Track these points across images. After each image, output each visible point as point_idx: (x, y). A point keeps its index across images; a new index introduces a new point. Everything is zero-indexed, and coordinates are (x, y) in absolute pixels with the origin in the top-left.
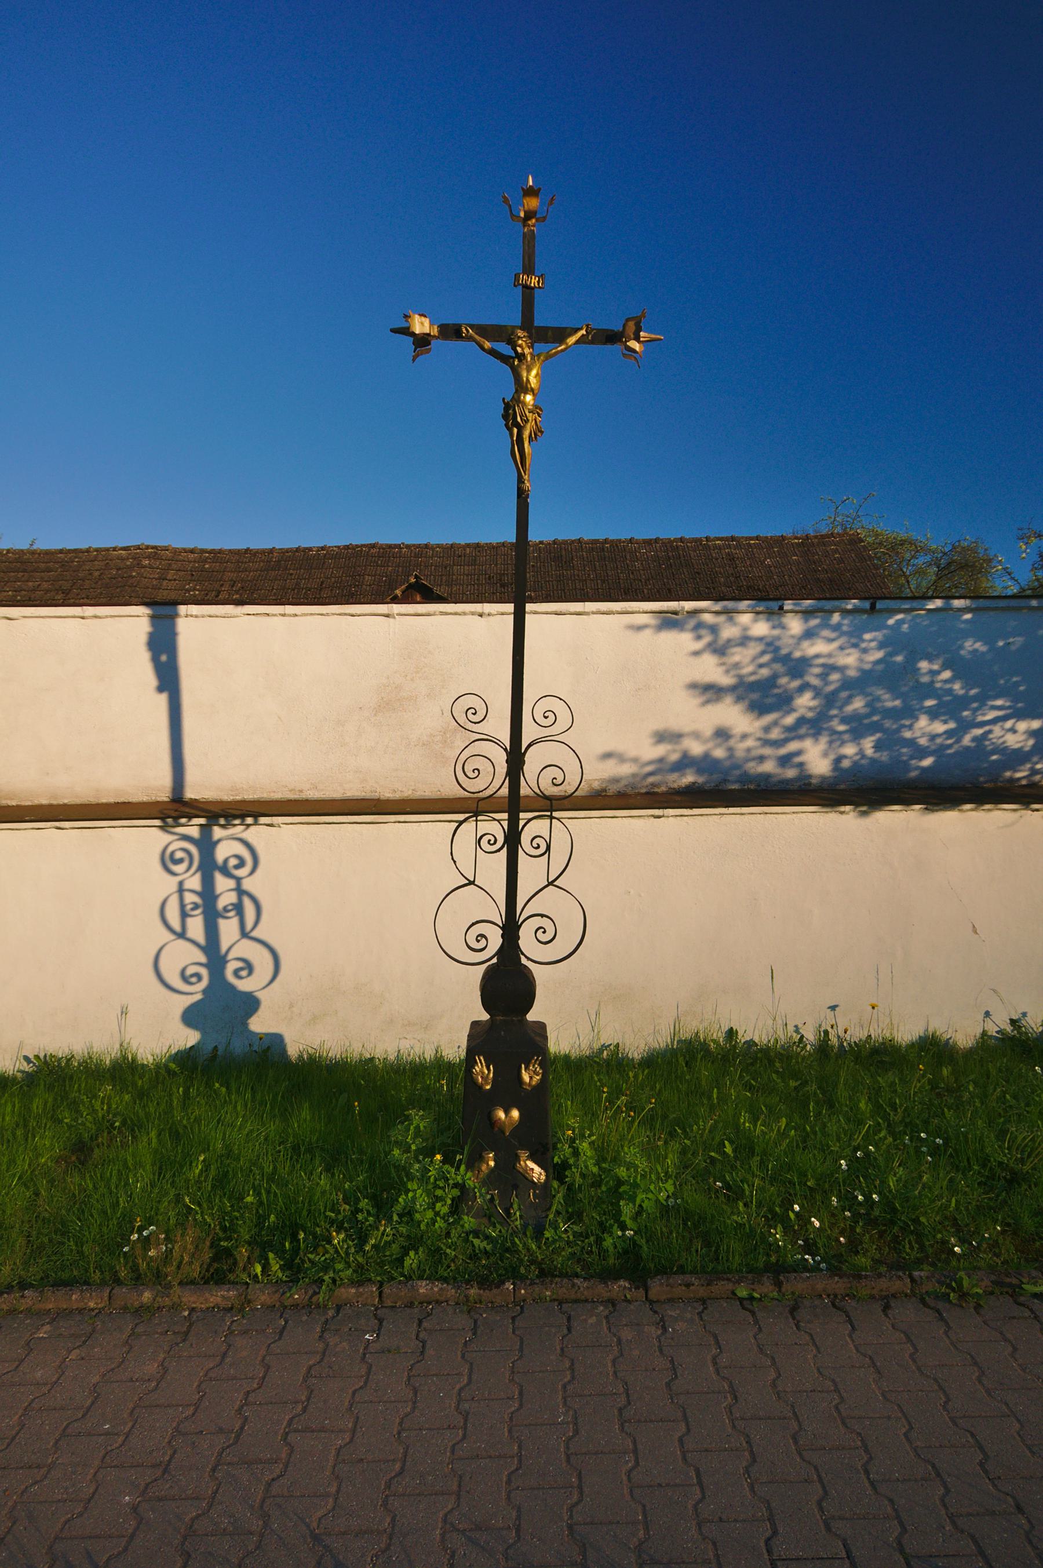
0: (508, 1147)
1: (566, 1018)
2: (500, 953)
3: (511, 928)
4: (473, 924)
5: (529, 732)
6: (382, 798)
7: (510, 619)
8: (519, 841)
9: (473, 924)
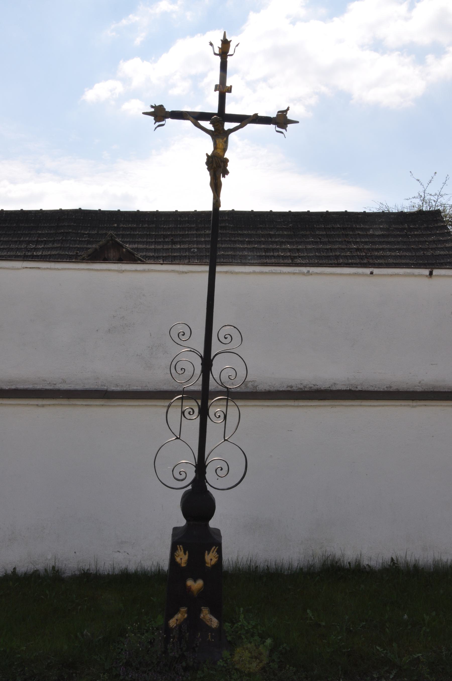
0: (194, 603)
1: (242, 536)
2: (194, 482)
3: (201, 466)
4: (173, 471)
5: (216, 347)
6: (109, 389)
7: (206, 277)
8: (207, 414)
9: (173, 471)
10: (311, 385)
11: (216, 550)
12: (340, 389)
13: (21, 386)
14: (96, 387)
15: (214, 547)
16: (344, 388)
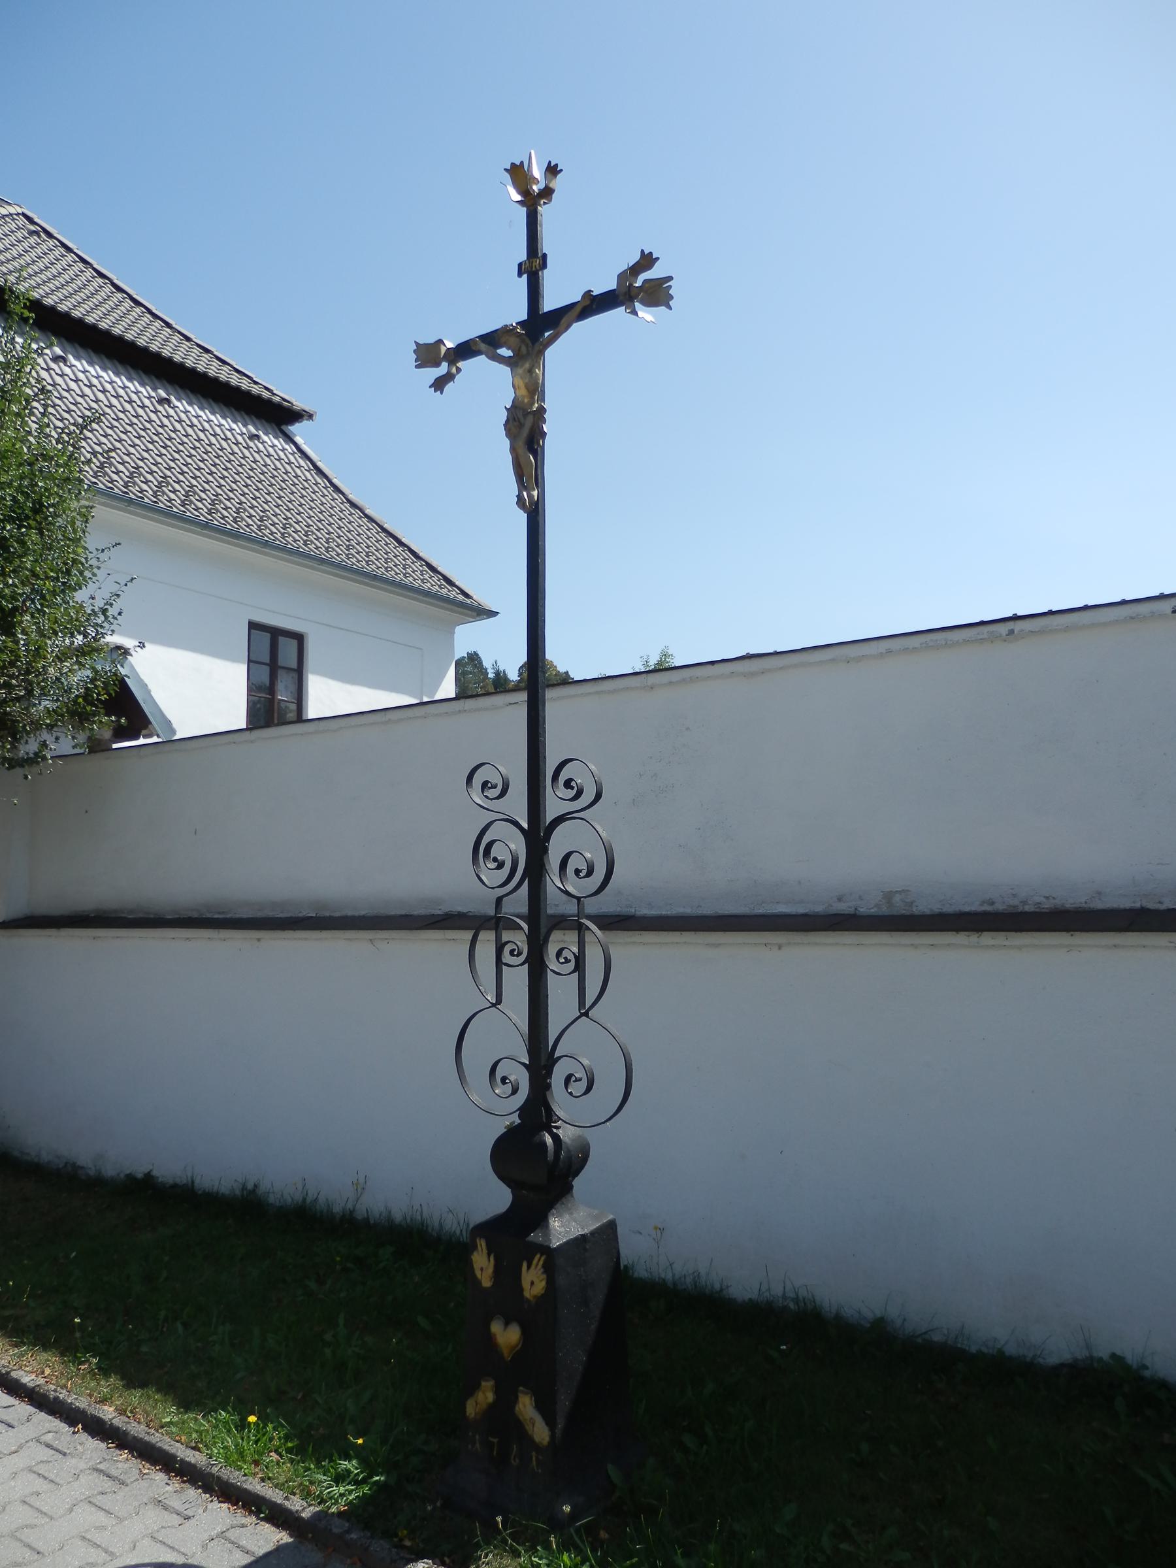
10: (1038, 899)
11: (541, 1263)
12: (1115, 906)
13: (961, 938)
14: (619, 909)
15: (538, 1256)
16: (1126, 904)
